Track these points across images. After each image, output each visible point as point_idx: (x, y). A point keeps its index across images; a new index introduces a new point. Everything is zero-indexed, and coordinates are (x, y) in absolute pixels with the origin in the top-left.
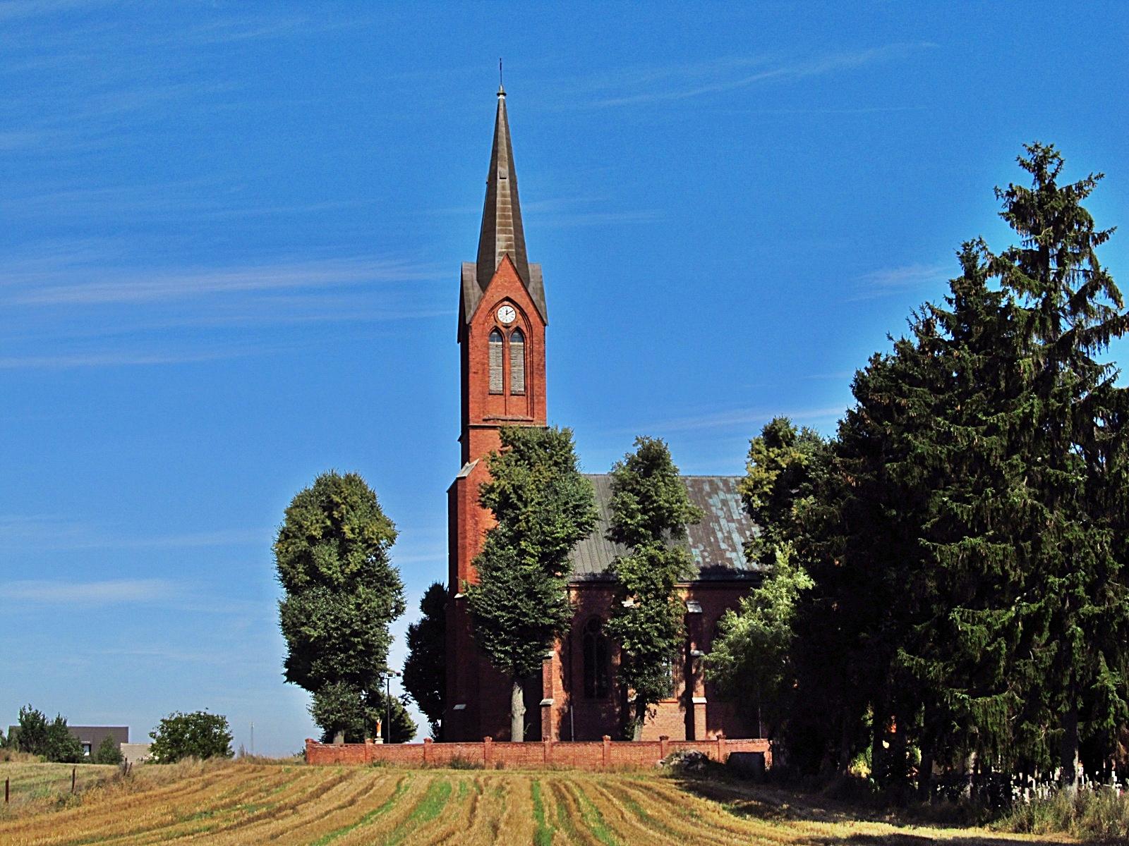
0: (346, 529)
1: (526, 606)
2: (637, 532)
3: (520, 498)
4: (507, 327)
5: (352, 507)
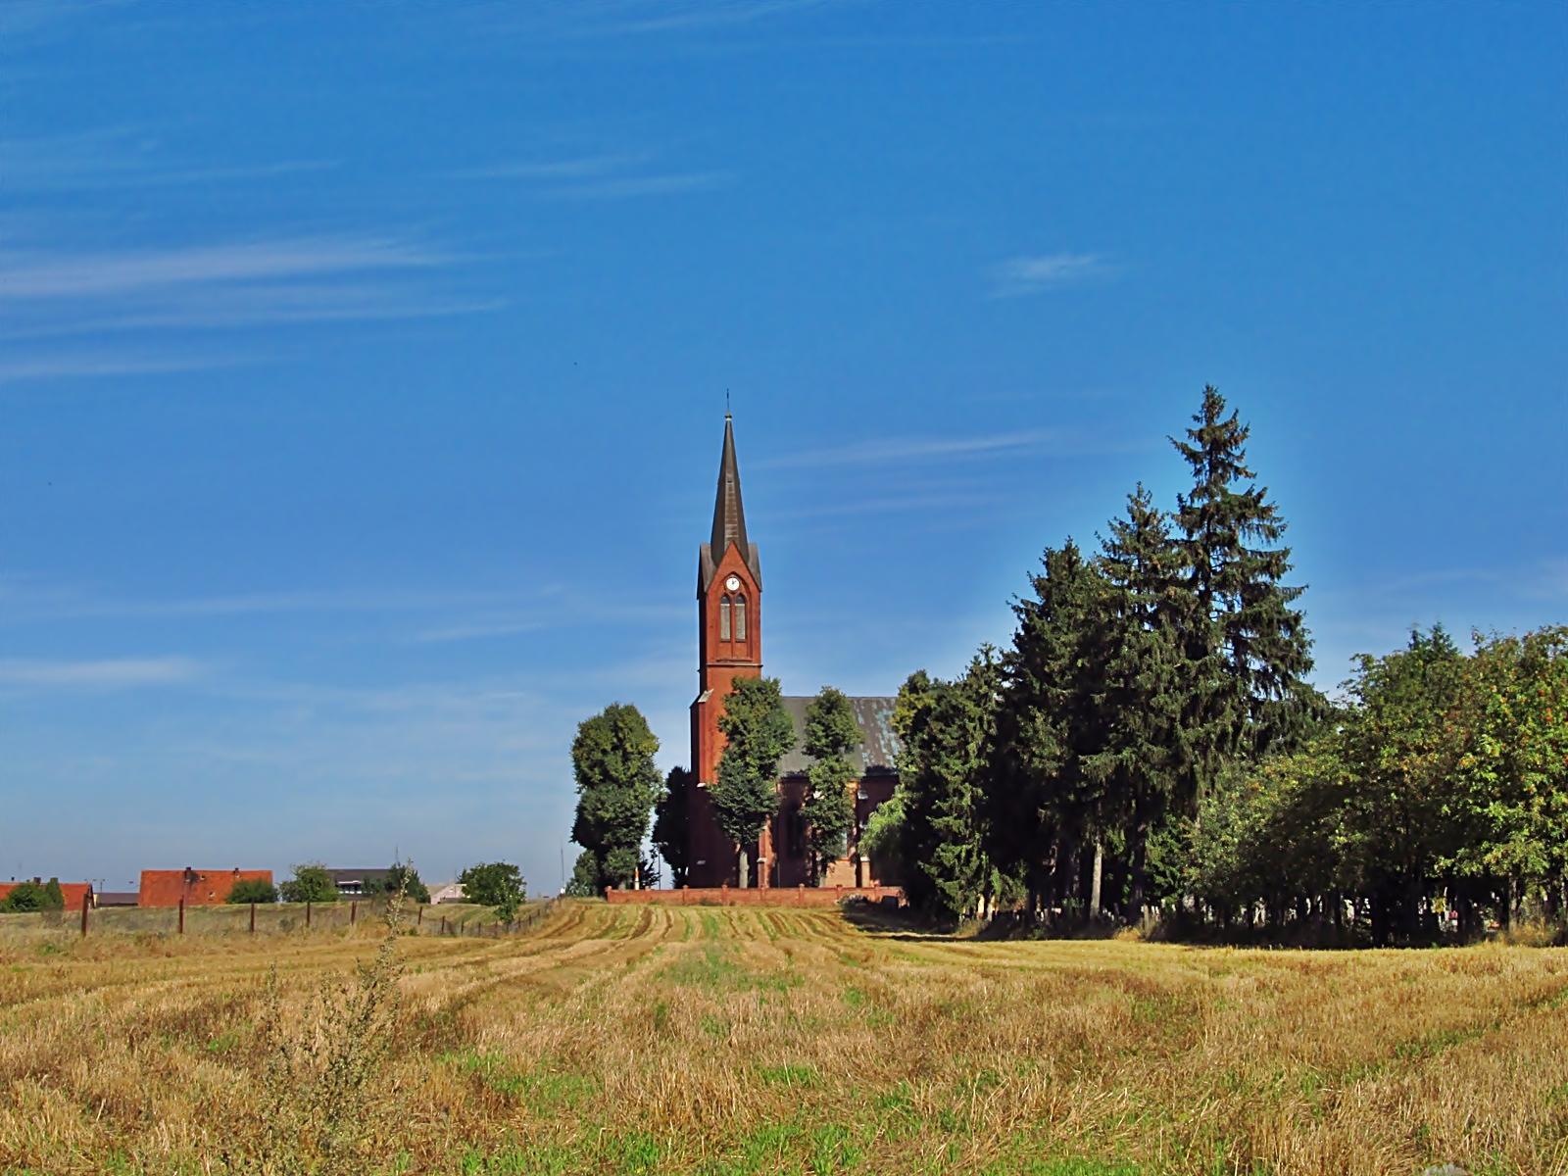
0: (628, 745)
1: (750, 799)
2: (822, 750)
3: (745, 728)
4: (733, 592)
5: (631, 730)
